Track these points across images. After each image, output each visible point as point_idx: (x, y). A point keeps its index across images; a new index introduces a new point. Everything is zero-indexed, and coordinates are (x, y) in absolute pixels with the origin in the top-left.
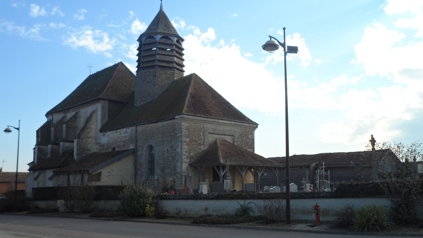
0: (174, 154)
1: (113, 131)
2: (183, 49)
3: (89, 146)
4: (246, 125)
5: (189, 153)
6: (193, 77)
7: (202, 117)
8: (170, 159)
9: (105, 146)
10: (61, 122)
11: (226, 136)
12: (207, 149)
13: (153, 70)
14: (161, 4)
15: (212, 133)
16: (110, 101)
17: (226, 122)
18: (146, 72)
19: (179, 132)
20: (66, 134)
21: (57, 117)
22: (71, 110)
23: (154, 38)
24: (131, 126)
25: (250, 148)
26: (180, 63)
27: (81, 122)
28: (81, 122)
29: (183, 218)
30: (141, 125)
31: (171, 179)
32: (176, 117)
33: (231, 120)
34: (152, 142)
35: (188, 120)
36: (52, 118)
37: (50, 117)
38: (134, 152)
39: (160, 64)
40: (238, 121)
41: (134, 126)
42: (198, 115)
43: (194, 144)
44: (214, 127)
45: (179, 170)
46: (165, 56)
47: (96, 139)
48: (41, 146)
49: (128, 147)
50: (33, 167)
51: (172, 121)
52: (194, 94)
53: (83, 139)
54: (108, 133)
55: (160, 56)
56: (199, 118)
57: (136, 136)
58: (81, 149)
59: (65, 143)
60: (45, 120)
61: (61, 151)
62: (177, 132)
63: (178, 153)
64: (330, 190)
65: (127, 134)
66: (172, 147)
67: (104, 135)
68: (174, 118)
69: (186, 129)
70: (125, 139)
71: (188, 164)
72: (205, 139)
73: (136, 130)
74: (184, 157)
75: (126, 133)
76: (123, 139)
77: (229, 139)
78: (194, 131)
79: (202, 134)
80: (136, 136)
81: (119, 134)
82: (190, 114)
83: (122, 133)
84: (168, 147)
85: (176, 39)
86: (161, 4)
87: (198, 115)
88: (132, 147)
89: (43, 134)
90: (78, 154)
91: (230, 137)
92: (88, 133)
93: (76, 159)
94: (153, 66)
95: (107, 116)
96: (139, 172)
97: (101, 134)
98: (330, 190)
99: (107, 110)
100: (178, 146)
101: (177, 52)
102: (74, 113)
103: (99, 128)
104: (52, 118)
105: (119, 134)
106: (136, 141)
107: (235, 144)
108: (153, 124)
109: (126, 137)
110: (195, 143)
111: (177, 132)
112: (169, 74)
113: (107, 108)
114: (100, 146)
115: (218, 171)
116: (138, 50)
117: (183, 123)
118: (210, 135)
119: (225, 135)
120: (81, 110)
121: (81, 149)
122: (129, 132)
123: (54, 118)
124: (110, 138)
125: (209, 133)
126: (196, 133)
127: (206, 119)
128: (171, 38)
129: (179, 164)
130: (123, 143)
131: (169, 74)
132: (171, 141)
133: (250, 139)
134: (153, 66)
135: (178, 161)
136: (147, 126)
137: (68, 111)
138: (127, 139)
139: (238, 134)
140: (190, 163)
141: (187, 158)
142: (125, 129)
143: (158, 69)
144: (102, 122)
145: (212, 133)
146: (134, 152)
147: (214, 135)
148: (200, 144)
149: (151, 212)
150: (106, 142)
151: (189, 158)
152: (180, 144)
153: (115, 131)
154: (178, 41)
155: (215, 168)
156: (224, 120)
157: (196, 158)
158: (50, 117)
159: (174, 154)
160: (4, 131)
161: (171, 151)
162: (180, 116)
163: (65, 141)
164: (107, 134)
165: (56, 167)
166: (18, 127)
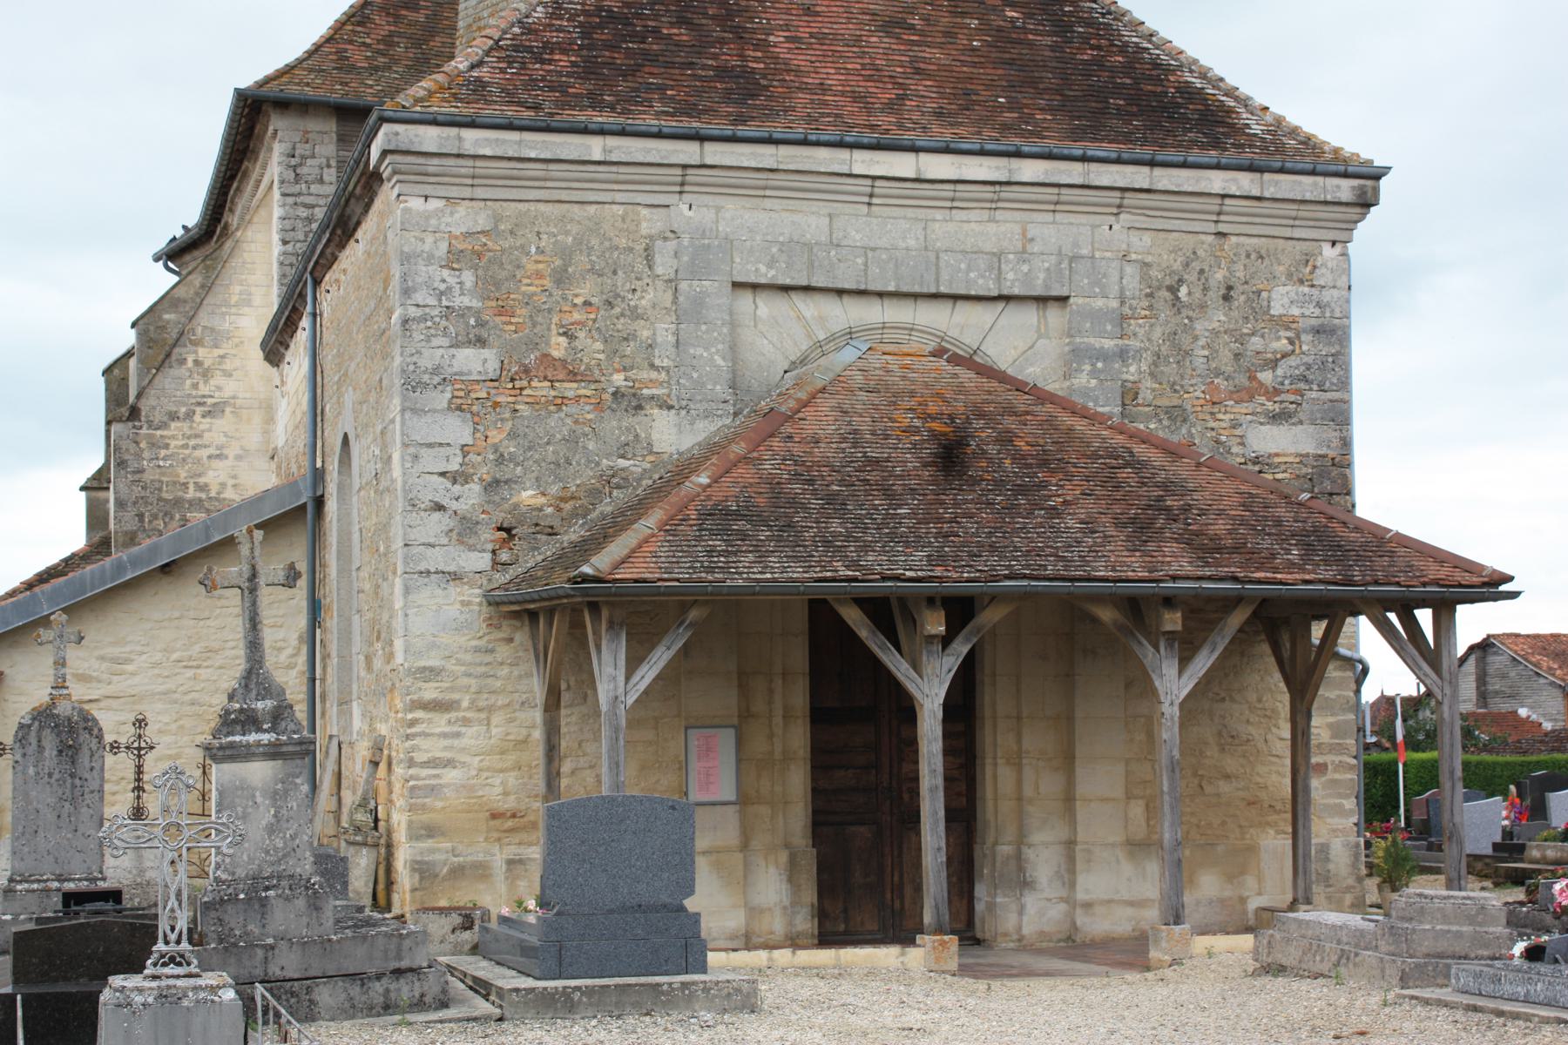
4: (1217, 181)
5: (492, 486)
11: (966, 312)
15: (786, 289)
42: (581, 117)
44: (809, 221)
56: (595, 147)
69: (454, 260)
71: (474, 594)
78: (561, 278)
82: (600, 119)
87: (581, 117)
91: (1028, 316)
92: (206, 374)
110: (570, 389)
118: (766, 307)
119: (956, 298)
126: (585, 290)
127: (687, 152)
133: (1285, 323)
140: (501, 578)
141: (465, 529)
147: (809, 307)
151: (488, 536)
155: (853, 616)
156: (914, 149)
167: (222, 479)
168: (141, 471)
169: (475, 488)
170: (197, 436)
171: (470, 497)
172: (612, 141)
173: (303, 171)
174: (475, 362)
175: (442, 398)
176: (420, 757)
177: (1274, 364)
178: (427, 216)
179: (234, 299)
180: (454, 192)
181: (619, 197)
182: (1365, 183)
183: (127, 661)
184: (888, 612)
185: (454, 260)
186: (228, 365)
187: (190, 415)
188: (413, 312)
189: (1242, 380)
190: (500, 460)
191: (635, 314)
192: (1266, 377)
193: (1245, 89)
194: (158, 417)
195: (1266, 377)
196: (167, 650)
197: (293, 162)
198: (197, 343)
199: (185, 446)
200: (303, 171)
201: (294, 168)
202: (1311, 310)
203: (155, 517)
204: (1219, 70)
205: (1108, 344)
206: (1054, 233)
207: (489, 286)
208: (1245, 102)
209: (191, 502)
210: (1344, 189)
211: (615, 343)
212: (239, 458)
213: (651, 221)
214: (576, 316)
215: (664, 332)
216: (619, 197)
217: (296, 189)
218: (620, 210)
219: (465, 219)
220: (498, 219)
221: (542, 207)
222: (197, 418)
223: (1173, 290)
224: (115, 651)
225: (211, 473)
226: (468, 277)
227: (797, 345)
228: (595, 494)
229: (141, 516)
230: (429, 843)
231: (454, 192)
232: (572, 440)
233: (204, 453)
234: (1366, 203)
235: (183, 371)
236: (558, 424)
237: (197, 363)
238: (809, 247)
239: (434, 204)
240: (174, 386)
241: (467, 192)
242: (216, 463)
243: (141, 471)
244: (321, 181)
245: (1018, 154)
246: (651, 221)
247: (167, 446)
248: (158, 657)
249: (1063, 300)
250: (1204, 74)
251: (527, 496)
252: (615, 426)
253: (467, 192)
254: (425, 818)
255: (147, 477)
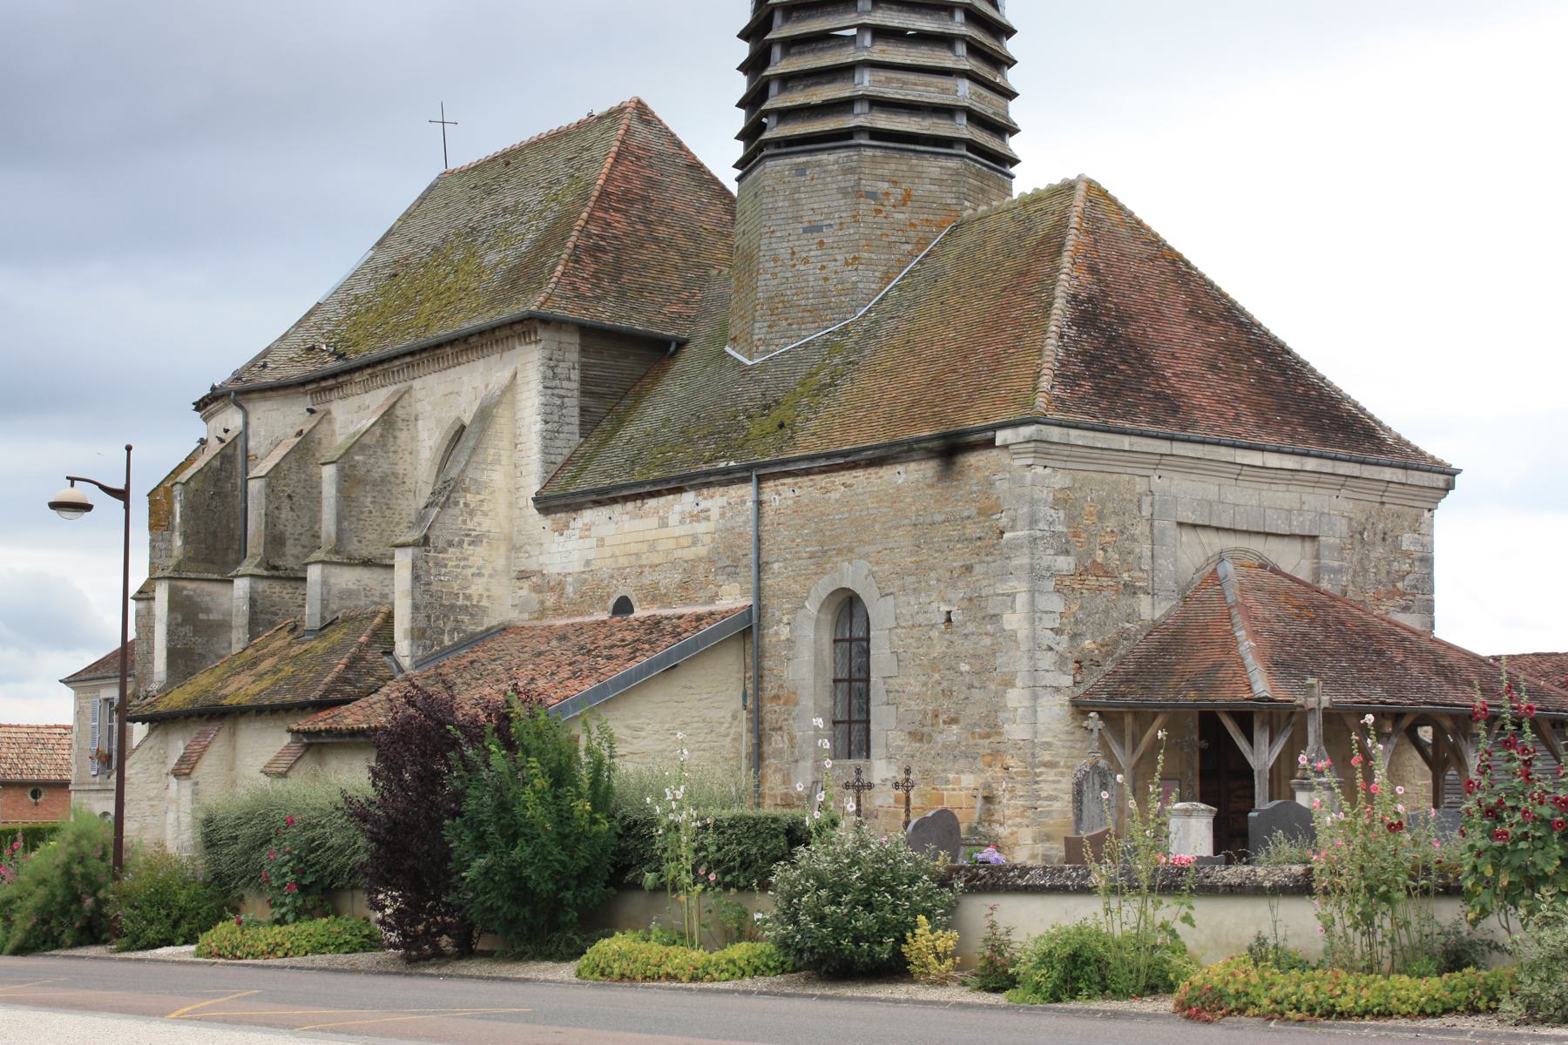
0: (987, 641)
1: (618, 508)
2: (1009, 32)
3: (476, 589)
4: (1388, 474)
6: (1093, 210)
7: (1142, 435)
8: (964, 667)
9: (569, 589)
11: (1272, 542)
12: (1167, 615)
13: (843, 154)
16: (593, 335)
17: (1273, 460)
19: (1014, 520)
20: (340, 518)
22: (357, 377)
25: (1405, 609)
26: (989, 112)
27: (424, 443)
31: (969, 780)
33: (1300, 447)
34: (852, 575)
35: (1066, 451)
36: (246, 424)
38: (746, 631)
39: (884, 121)
40: (1342, 453)
41: (746, 480)
42: (1120, 423)
43: (1100, 589)
44: (1208, 488)
47: (515, 548)
49: (712, 599)
52: (1090, 299)
53: (444, 551)
56: (1126, 442)
58: (435, 610)
61: (312, 616)
63: (1013, 637)
65: (701, 528)
66: (973, 602)
69: (1056, 504)
70: (689, 554)
71: (1064, 700)
73: (759, 503)
75: (700, 516)
76: (679, 554)
77: (1292, 560)
78: (1101, 516)
79: (1141, 529)
81: (653, 522)
83: (674, 519)
84: (949, 602)
87: (1120, 423)
88: (733, 598)
90: (417, 635)
91: (1296, 546)
92: (472, 513)
94: (842, 137)
95: (576, 421)
96: (777, 742)
97: (547, 522)
99: (575, 385)
100: (1012, 596)
103: (533, 485)
104: (246, 424)
105: (653, 522)
106: (760, 568)
107: (1325, 585)
108: (860, 473)
109: (695, 540)
110: (1105, 581)
112: (933, 181)
113: (575, 375)
114: (537, 589)
115: (1242, 744)
116: (745, 35)
118: (1187, 536)
119: (1267, 534)
121: (435, 610)
122: (715, 513)
125: (1180, 524)
126: (1111, 524)
131: (933, 181)
132: (969, 569)
133: (1408, 554)
135: (1009, 683)
136: (821, 480)
137: (339, 386)
138: (701, 551)
139: (1342, 527)
140: (1079, 691)
141: (1061, 662)
142: (689, 497)
143: (869, 152)
144: (546, 450)
145: (1194, 526)
146: (746, 631)
147: (1207, 537)
148: (1131, 589)
149: (938, 957)
150: (576, 567)
151: (1072, 666)
153: (630, 506)
157: (1109, 666)
161: (971, 627)
163: (343, 557)
167: (481, 591)
168: (429, 584)
169: (1066, 637)
170: (465, 559)
171: (1063, 643)
172: (1134, 439)
173: (558, 370)
174: (1065, 564)
175: (1050, 585)
176: (1043, 794)
177: (1403, 578)
178: (1044, 477)
179: (490, 458)
180: (1058, 464)
181: (1129, 470)
182: (1450, 474)
183: (642, 729)
184: (1245, 718)
185: (1056, 504)
186: (485, 508)
187: (461, 543)
188: (1039, 534)
189: (1390, 587)
190: (1076, 622)
191: (1133, 539)
192: (1400, 585)
193: (1378, 416)
194: (441, 544)
195: (1400, 585)
196: (662, 723)
197: (552, 363)
198: (466, 490)
199: (457, 566)
200: (558, 370)
201: (552, 368)
202: (1419, 548)
203: (438, 618)
204: (1362, 404)
205: (1336, 564)
206: (1316, 500)
207: (1071, 520)
208: (1379, 423)
209: (461, 608)
210: (1440, 480)
211: (1125, 554)
212: (491, 576)
213: (1141, 485)
214: (1108, 539)
215: (1145, 549)
216: (1129, 470)
217: (554, 384)
218: (1127, 477)
219: (1060, 480)
220: (1074, 480)
221: (1095, 475)
222: (465, 545)
223: (1361, 534)
224: (633, 722)
225: (474, 587)
226: (1062, 514)
227: (1199, 559)
228: (1116, 643)
229: (429, 617)
230: (1047, 845)
231: (1058, 464)
232: (1106, 612)
233: (469, 572)
234: (1449, 486)
235: (456, 511)
236: (1100, 602)
237: (466, 505)
238: (1210, 503)
239: (1048, 471)
240: (453, 521)
241: (1063, 465)
242: (478, 580)
243: (429, 584)
244: (569, 379)
245: (1307, 455)
246: (1141, 485)
247: (446, 566)
248: (657, 727)
249: (1314, 538)
250: (1356, 405)
251: (1087, 643)
252: (1124, 602)
253: (1063, 465)
254: (1046, 829)
255: (434, 588)
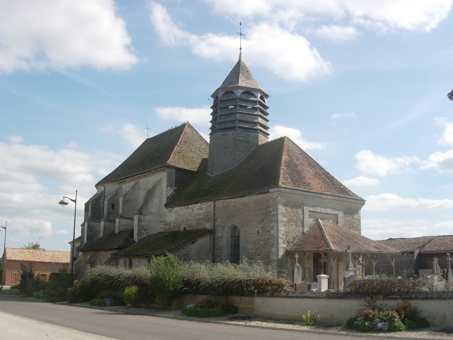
8: (262, 243)
9: (172, 225)
10: (116, 194)
13: (233, 132)
14: (240, 53)
18: (224, 135)
21: (111, 188)
23: (232, 92)
24: (207, 200)
28: (141, 196)
29: (297, 321)
30: (221, 199)
32: (271, 190)
34: (236, 222)
37: (102, 188)
38: (211, 232)
41: (212, 201)
45: (274, 257)
46: (248, 116)
48: (90, 223)
50: (78, 247)
51: (264, 195)
54: (176, 209)
55: (241, 115)
57: (214, 214)
59: (122, 220)
60: (95, 191)
62: (271, 209)
63: (273, 236)
64: (427, 289)
65: (201, 211)
66: (264, 228)
67: (170, 212)
68: (268, 192)
72: (305, 219)
73: (215, 206)
74: (281, 241)
80: (214, 214)
81: (191, 210)
83: (195, 209)
84: (258, 228)
85: (259, 95)
86: (240, 53)
89: (94, 208)
93: (136, 240)
97: (167, 210)
98: (427, 289)
99: (174, 181)
100: (273, 226)
101: (261, 111)
102: (132, 183)
108: (237, 199)
109: (200, 214)
111: (271, 209)
113: (174, 179)
114: (165, 225)
116: (212, 108)
117: (279, 198)
120: (140, 181)
122: (205, 208)
123: (106, 188)
124: (179, 215)
128: (254, 93)
129: (273, 249)
130: (196, 222)
132: (263, 220)
134: (233, 128)
136: (229, 201)
137: (124, 181)
138: (201, 216)
142: (199, 205)
143: (239, 131)
152: (276, 224)
153: (185, 207)
154: (262, 98)
158: (102, 188)
159: (267, 237)
160: (60, 203)
161: (263, 234)
162: (276, 189)
164: (174, 210)
165: (116, 249)
166: (75, 199)
